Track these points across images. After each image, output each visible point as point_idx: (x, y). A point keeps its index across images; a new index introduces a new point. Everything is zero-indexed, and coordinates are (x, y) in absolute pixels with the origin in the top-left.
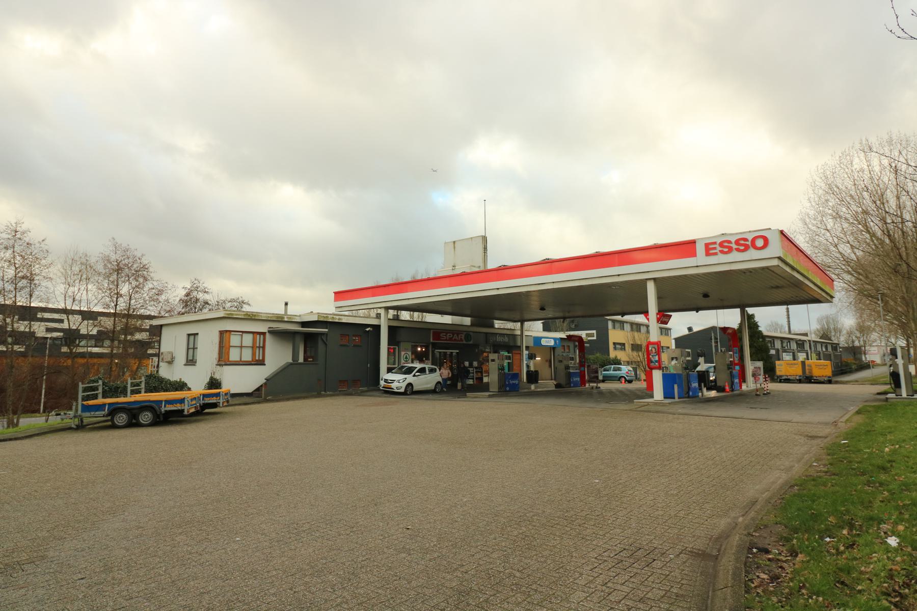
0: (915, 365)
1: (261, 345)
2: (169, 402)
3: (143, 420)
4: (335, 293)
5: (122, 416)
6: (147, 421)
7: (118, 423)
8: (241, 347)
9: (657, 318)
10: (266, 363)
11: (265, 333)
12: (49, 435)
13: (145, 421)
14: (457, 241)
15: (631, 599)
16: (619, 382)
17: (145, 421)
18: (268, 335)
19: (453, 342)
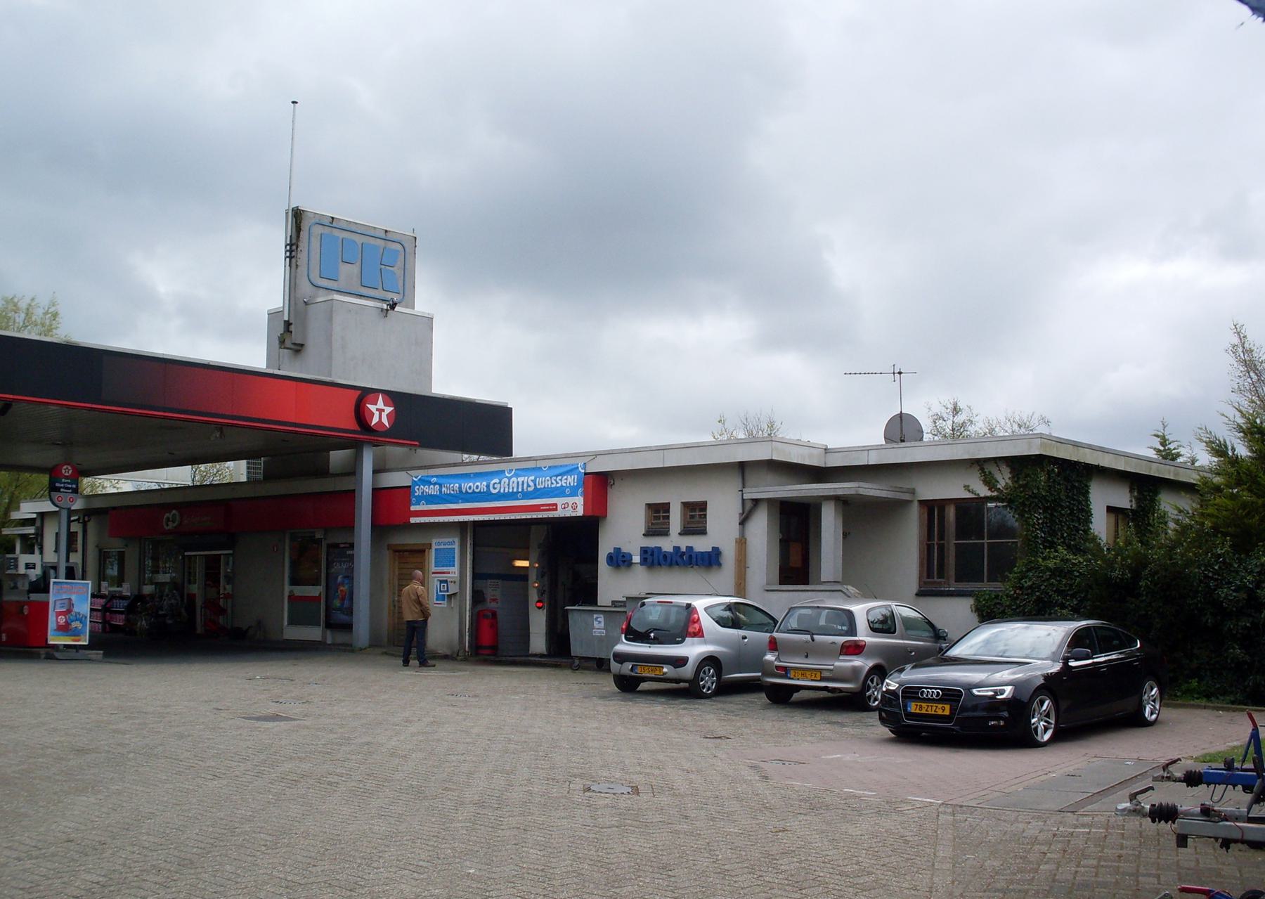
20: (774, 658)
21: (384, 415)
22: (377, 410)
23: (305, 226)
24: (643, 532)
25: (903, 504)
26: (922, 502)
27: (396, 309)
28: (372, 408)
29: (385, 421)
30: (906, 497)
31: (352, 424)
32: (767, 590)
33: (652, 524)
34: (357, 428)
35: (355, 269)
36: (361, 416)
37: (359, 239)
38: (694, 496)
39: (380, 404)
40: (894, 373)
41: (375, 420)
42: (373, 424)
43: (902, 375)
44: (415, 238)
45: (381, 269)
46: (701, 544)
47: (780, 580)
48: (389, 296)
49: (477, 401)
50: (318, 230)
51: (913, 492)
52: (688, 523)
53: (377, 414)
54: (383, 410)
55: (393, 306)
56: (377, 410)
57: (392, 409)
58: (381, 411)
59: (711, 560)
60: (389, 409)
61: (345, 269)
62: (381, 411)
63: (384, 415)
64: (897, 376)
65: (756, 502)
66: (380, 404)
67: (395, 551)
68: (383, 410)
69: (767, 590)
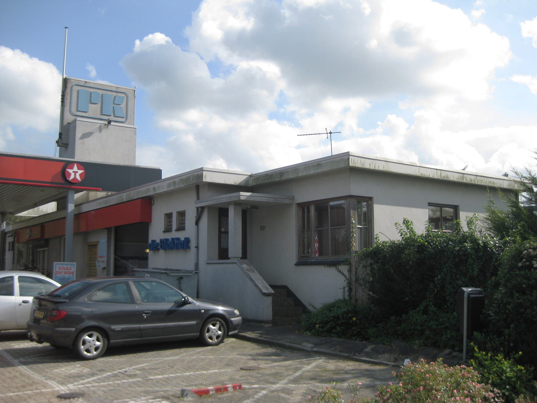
20: (42, 317)
22: (73, 172)
23: (69, 86)
24: (163, 230)
25: (288, 206)
26: (299, 205)
27: (111, 124)
28: (70, 171)
29: (78, 177)
30: (287, 201)
31: (60, 180)
32: (208, 264)
33: (168, 226)
34: (63, 182)
35: (98, 106)
36: (64, 175)
37: (101, 92)
38: (181, 209)
39: (75, 168)
40: (327, 133)
41: (72, 177)
43: (326, 134)
44: (135, 91)
45: (114, 107)
46: (182, 235)
47: (219, 256)
48: (107, 118)
49: (140, 167)
50: (76, 88)
51: (293, 198)
52: (181, 224)
54: (77, 172)
55: (109, 122)
56: (73, 172)
58: (75, 172)
59: (185, 245)
60: (80, 172)
61: (92, 106)
62: (75, 172)
64: (329, 135)
65: (203, 208)
66: (75, 168)
67: (90, 246)
68: (77, 172)
69: (208, 264)
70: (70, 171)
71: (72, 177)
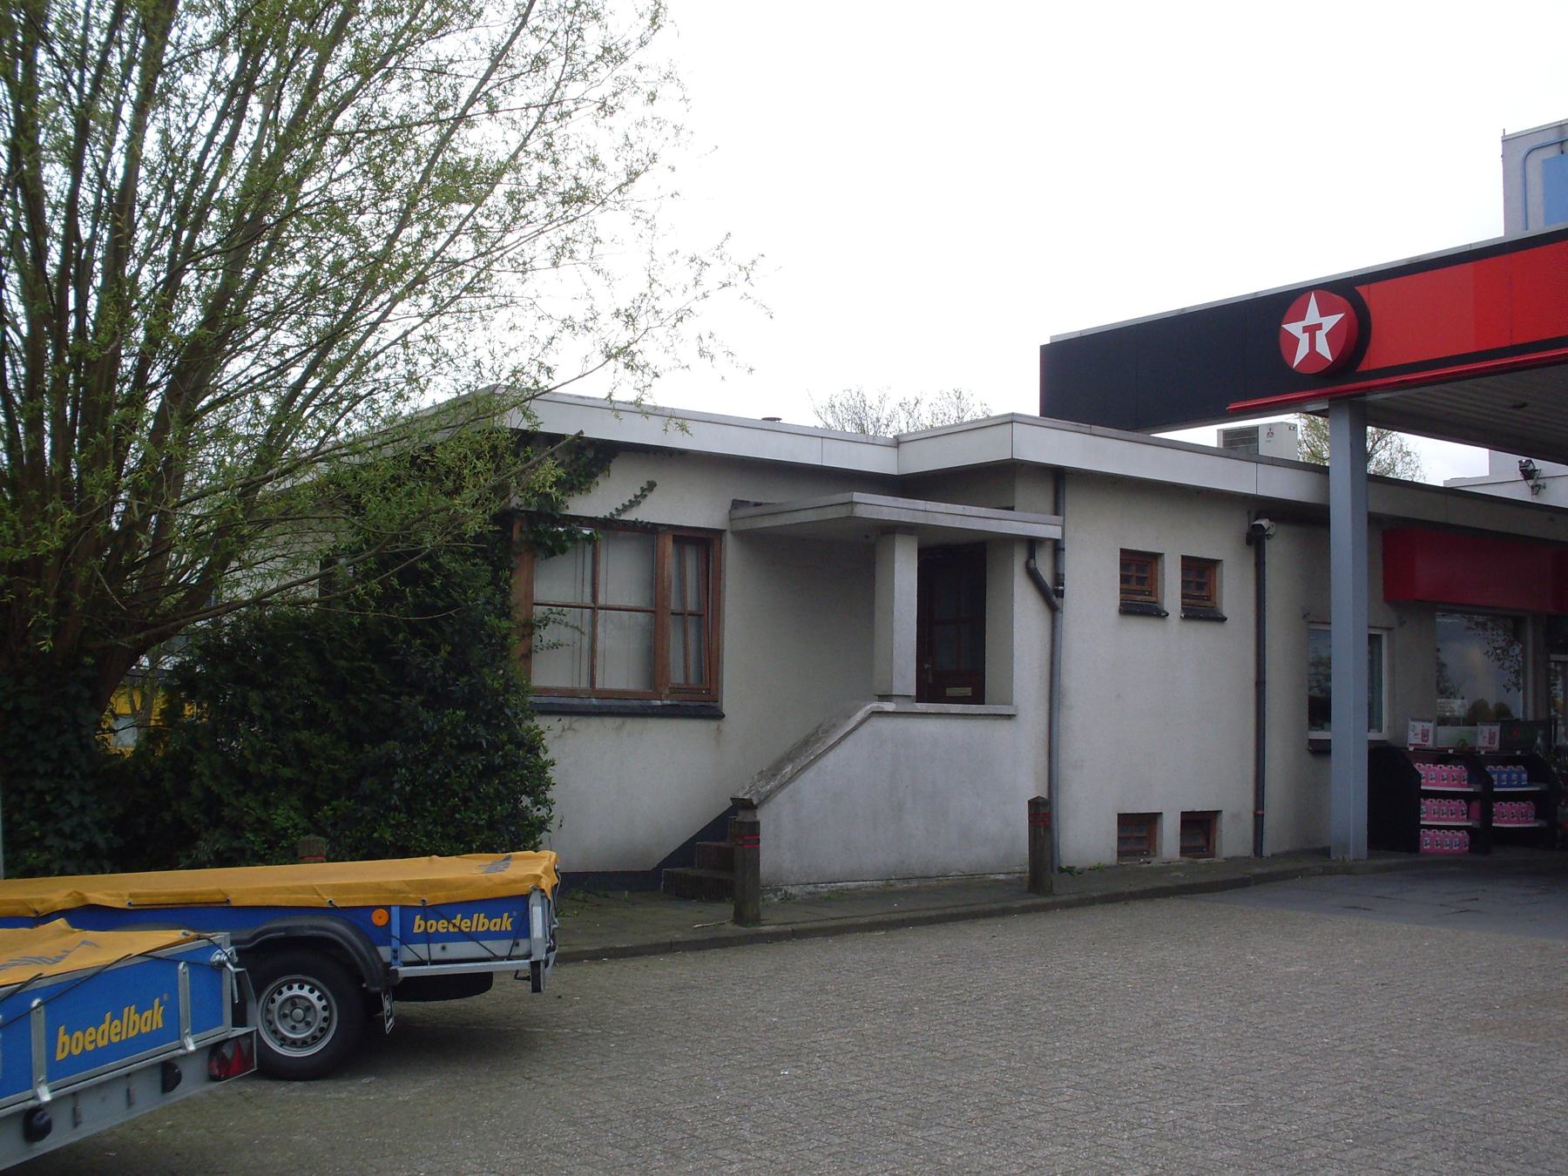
0: (1115, 867)
1: (691, 605)
2: (312, 928)
3: (294, 1043)
4: (1183, 557)
5: (293, 1001)
6: (315, 1039)
7: (284, 1041)
8: (595, 608)
9: (1285, 303)
10: (727, 705)
11: (718, 534)
12: (1139, 904)
13: (304, 1043)
14: (1367, 508)
15: (1523, 1047)
16: (715, 916)
17: (304, 1043)
18: (732, 557)
19: (1513, 789)
21: (1321, 337)
22: (1306, 329)
28: (1294, 328)
29: (1323, 349)
41: (1302, 351)
42: (1295, 365)
53: (1304, 339)
54: (1319, 327)
56: (1306, 329)
57: (1284, 326)
58: (1312, 330)
60: (1330, 321)
62: (1312, 330)
63: (1321, 337)
66: (1313, 315)
68: (1319, 327)
70: (1294, 328)
71: (1302, 351)
